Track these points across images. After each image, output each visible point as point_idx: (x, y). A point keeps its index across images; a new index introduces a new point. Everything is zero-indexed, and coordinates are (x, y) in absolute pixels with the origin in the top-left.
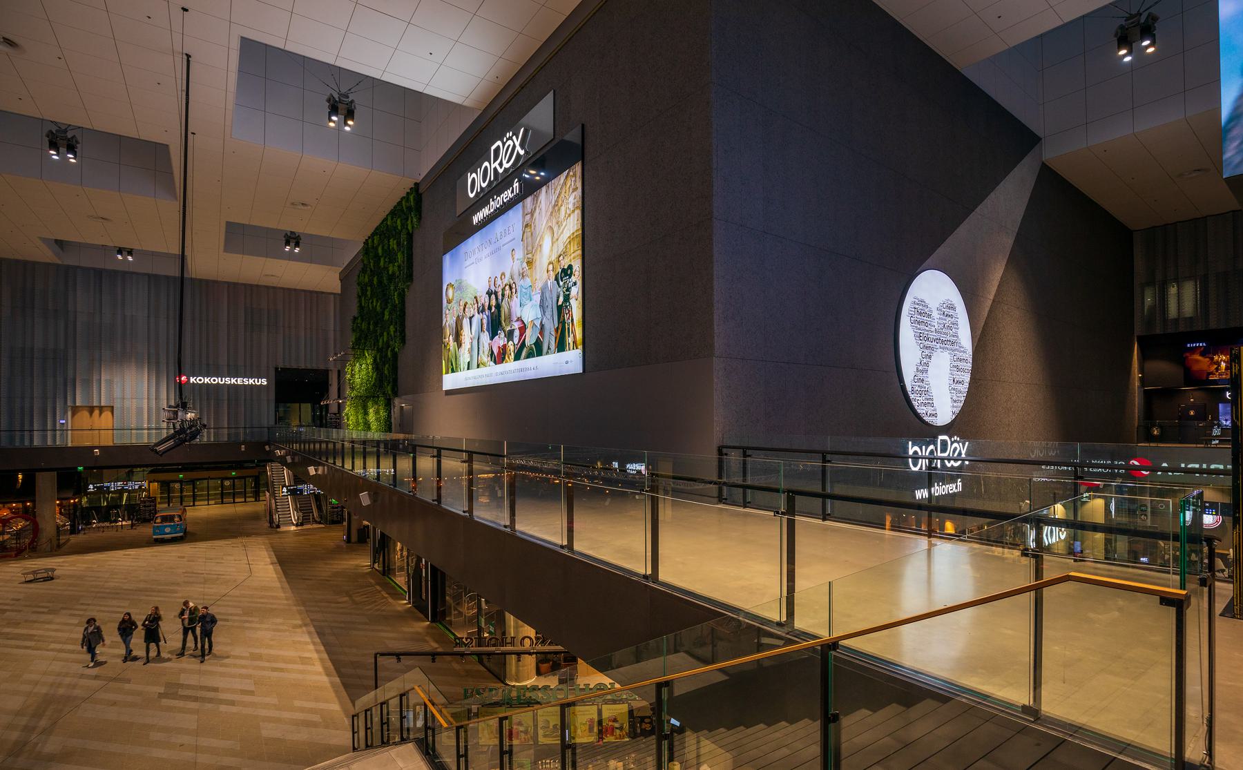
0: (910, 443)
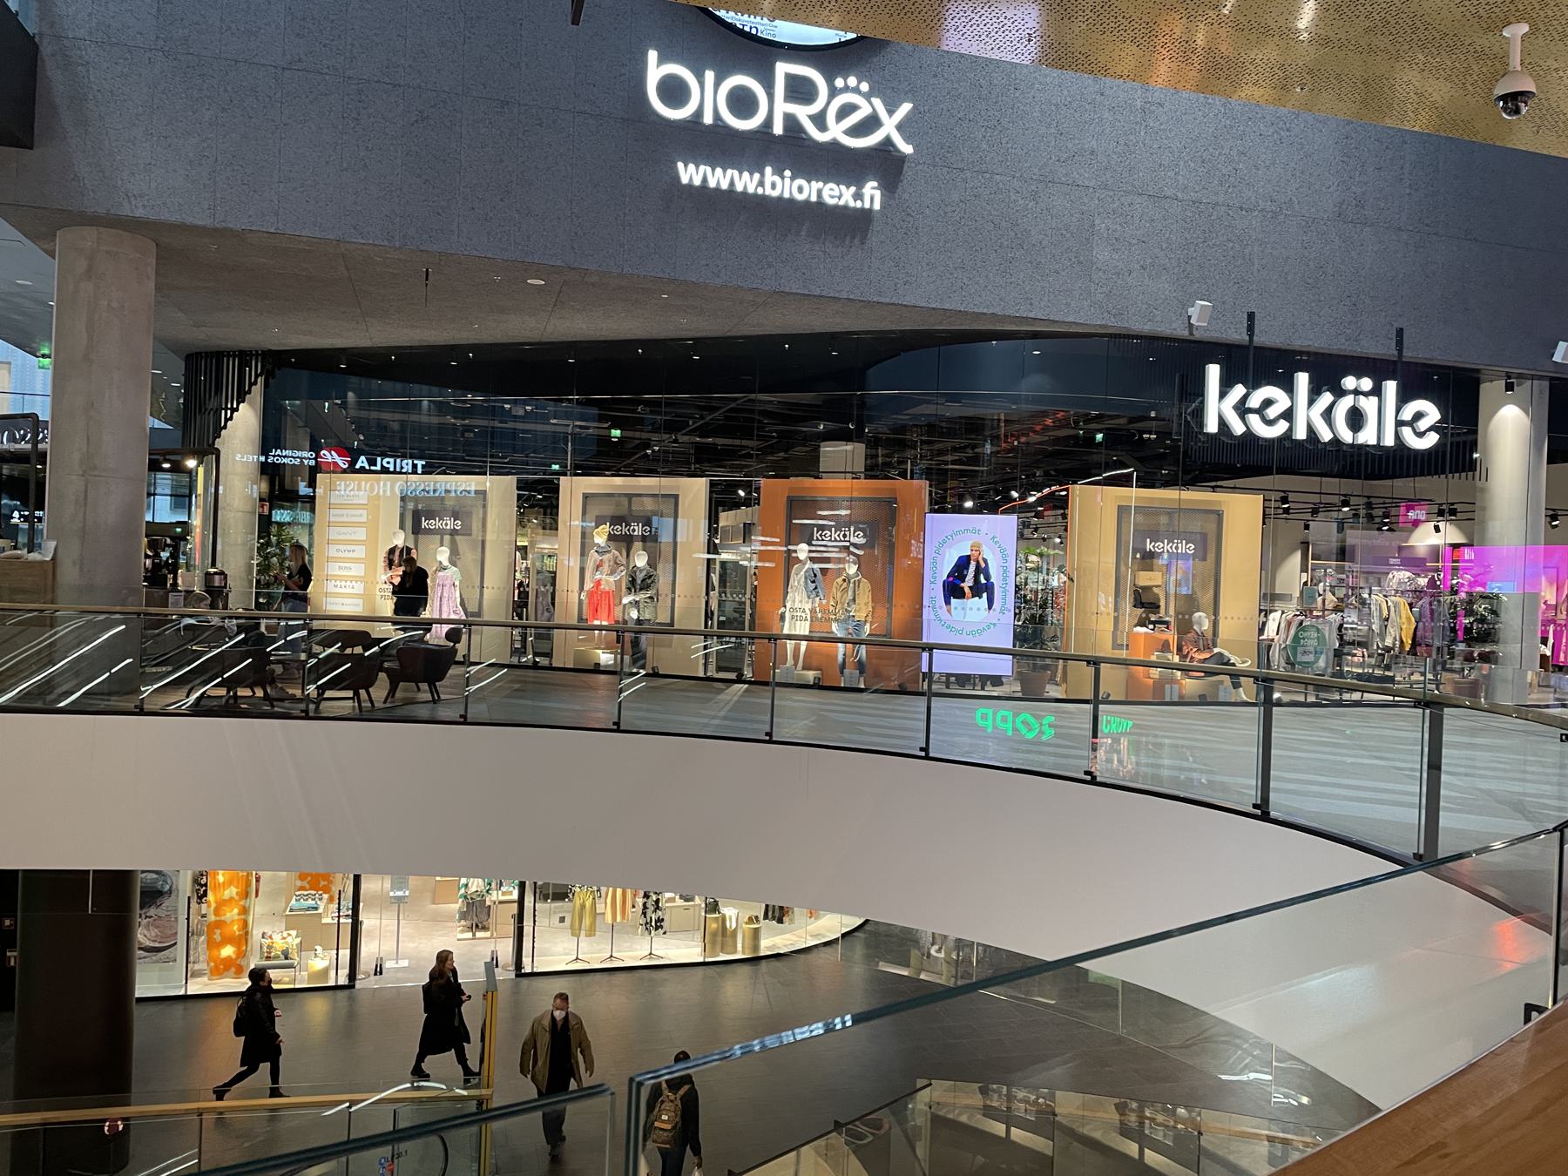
0: (1213, 372)
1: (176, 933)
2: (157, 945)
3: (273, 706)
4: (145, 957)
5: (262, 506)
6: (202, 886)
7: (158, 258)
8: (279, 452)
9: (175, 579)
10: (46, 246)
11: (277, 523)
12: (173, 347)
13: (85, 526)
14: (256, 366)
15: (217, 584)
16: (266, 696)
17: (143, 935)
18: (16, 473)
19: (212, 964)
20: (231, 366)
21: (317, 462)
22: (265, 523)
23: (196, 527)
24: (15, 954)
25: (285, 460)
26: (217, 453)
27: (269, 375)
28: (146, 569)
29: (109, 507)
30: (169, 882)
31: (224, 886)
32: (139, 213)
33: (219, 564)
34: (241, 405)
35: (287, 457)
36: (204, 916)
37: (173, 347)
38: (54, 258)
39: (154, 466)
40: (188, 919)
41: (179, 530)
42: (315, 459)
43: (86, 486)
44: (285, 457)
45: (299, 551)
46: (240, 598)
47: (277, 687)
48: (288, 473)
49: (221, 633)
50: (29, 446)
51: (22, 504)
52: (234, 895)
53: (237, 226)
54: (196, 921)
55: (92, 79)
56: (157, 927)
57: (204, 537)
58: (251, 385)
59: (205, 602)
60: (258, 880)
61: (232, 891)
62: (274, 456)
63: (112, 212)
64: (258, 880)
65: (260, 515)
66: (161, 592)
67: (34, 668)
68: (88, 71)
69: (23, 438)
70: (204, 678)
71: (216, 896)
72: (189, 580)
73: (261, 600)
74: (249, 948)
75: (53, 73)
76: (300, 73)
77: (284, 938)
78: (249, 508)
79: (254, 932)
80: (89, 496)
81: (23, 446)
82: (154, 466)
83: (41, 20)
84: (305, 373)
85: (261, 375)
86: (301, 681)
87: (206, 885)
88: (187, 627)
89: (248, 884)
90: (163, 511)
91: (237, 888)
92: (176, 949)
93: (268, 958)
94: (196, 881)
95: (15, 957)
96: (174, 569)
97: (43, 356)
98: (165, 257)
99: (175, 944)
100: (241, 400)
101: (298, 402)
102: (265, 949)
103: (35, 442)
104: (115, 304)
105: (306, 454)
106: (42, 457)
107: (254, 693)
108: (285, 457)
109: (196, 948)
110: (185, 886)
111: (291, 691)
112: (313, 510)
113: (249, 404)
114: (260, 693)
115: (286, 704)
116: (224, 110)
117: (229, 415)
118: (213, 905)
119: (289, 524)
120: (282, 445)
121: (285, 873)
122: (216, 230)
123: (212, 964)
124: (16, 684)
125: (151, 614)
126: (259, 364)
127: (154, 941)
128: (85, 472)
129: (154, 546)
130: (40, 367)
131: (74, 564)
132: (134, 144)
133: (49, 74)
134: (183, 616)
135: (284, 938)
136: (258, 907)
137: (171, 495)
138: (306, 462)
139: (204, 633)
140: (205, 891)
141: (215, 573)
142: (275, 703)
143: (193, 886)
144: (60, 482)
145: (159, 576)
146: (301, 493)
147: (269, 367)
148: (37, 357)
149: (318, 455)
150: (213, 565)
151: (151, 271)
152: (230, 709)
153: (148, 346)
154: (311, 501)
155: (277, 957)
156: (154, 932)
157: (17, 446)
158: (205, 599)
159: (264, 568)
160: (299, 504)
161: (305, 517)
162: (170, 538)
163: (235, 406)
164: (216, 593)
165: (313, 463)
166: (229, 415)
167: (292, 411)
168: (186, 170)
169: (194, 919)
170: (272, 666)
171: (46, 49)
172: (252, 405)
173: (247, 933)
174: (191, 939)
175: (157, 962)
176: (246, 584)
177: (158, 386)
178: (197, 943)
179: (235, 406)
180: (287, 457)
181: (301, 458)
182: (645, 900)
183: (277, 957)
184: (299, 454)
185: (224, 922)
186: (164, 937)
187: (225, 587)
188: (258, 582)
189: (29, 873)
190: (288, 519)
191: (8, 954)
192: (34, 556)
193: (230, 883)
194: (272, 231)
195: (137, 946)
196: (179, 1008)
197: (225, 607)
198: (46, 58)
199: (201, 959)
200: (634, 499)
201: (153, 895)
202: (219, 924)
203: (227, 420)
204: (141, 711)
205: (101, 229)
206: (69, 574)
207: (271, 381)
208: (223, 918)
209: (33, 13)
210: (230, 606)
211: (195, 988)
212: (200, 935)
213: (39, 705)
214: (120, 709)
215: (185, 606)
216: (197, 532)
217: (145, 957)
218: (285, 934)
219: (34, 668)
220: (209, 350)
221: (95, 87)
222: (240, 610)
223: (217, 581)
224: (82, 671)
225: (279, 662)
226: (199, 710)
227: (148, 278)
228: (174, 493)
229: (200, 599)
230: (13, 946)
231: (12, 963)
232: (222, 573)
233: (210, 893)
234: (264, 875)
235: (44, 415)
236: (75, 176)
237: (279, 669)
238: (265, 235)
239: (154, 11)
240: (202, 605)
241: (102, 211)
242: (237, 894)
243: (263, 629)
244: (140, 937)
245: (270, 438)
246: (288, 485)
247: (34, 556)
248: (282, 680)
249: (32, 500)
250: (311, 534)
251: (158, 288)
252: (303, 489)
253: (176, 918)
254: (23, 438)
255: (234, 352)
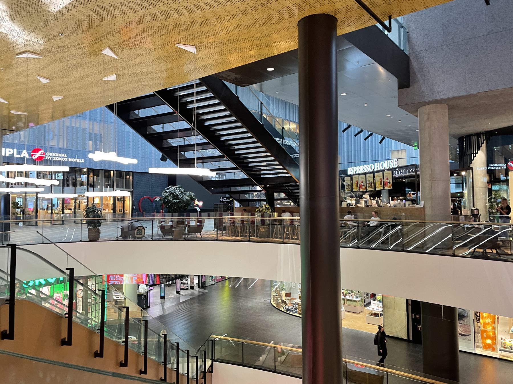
1: (470, 331)
2: (464, 334)
3: (500, 256)
4: (460, 337)
5: (489, 185)
6: (478, 316)
7: (449, 109)
8: (492, 165)
9: (461, 212)
10: (415, 114)
11: (494, 190)
12: (454, 137)
13: (432, 196)
14: (483, 137)
15: (475, 213)
16: (497, 253)
17: (460, 330)
18: (409, 181)
19: (484, 345)
20: (474, 139)
21: (507, 167)
22: (490, 191)
23: (466, 193)
24: (421, 327)
25: (494, 168)
26: (472, 169)
27: (488, 140)
28: (452, 209)
29: (439, 190)
30: (466, 313)
31: (486, 319)
32: (442, 97)
33: (475, 206)
34: (479, 151)
35: (496, 166)
36: (479, 327)
37: (454, 137)
38: (418, 117)
39: (452, 175)
40: (474, 327)
41: (459, 195)
42: (506, 166)
43: (432, 184)
44: (495, 166)
45: (504, 201)
46: (484, 217)
47: (501, 249)
48: (497, 172)
49: (479, 230)
50: (414, 173)
51: (411, 190)
52: (490, 322)
53: (475, 93)
54: (477, 328)
55: (425, 61)
56: (463, 328)
57: (469, 196)
58: (482, 144)
59: (472, 219)
60: (498, 318)
61: (489, 320)
62: (490, 167)
63: (434, 99)
64: (498, 318)
65: (488, 188)
66: (457, 216)
67: (419, 239)
68: (424, 59)
69: (412, 171)
70: (473, 244)
71: (483, 321)
72: (466, 212)
73: (491, 218)
74: (497, 342)
75: (414, 64)
76: (492, 35)
77: (510, 341)
78: (484, 186)
79: (498, 337)
80: (433, 187)
81: (412, 173)
82: (452, 175)
83: (410, 49)
84: (500, 136)
85: (485, 140)
86: (510, 247)
87: (479, 316)
88: (467, 228)
89: (494, 319)
90: (454, 189)
91: (491, 320)
92: (470, 337)
93: (504, 347)
94: (476, 314)
95: (420, 328)
96: (460, 208)
97: (415, 146)
98: (451, 108)
99: (470, 335)
100: (478, 149)
101: (499, 147)
102: (503, 344)
103: (416, 171)
104: (436, 127)
105: (503, 165)
106: (418, 176)
107: (492, 251)
108: (495, 166)
109: (477, 338)
110: (472, 316)
111: (506, 251)
112: (508, 185)
113: (481, 150)
114: (494, 251)
115: (505, 256)
116: (467, 56)
117: (474, 156)
118: (483, 324)
119: (499, 190)
120: (494, 163)
121: (508, 318)
122: (467, 96)
123: (484, 345)
124: (414, 244)
125: (455, 224)
126: (484, 137)
127: (463, 332)
128: (431, 179)
129: (453, 201)
130: (415, 150)
131: (430, 208)
132: (439, 76)
133: (413, 64)
134: (465, 224)
135: (510, 341)
136: (499, 328)
137: (455, 184)
138: (502, 167)
139: (470, 230)
140: (479, 318)
141: (475, 209)
142: (501, 255)
143: (475, 316)
144: (424, 184)
145: (456, 211)
146: (502, 179)
147: (488, 137)
148: (413, 146)
149: (507, 165)
150: (474, 206)
151: (447, 114)
152: (484, 256)
153: (447, 138)
154: (507, 182)
155: (507, 348)
156: (463, 329)
157: (411, 174)
158: (472, 218)
159: (491, 207)
160: (501, 183)
161: (505, 187)
162: (457, 198)
163: (476, 152)
164: (475, 216)
165: (505, 167)
166: (474, 156)
167: (497, 151)
168: (456, 79)
169: (476, 328)
170: (499, 242)
171: (411, 57)
172: (482, 151)
173: (495, 336)
174: (475, 334)
175: (464, 339)
176: (485, 212)
177: (451, 149)
178: (478, 336)
179: (476, 152)
180: (496, 166)
181: (501, 166)
182: (493, 330)
183: (507, 348)
184: (500, 165)
185: (487, 331)
186: (466, 332)
187: (478, 214)
188: (489, 212)
189: (424, 303)
190: (498, 188)
191: (418, 326)
192: (418, 206)
193: (488, 317)
194: (487, 90)
195: (458, 333)
196: (473, 357)
197: (479, 221)
198: (411, 60)
199: (480, 342)
200: (376, 174)
201: (462, 317)
202: (485, 331)
203: (474, 157)
204: (454, 255)
205: (431, 105)
206: (428, 211)
207: (489, 141)
208: (486, 329)
209: (408, 48)
210: (481, 220)
211: (478, 351)
212: (478, 333)
213: (421, 251)
214: (448, 254)
215: (465, 221)
216: (466, 197)
217: (460, 337)
218: (510, 340)
219: (419, 239)
220: (466, 135)
221: (426, 63)
222: (484, 222)
223: (475, 212)
224: (434, 240)
225: (501, 241)
226: (473, 256)
227: (446, 116)
228: (456, 183)
229: (470, 218)
230: (420, 324)
231: (420, 329)
232: (477, 209)
233: (481, 319)
234: (500, 317)
235: (418, 163)
236: (423, 91)
237: (501, 243)
238: (484, 93)
239: (442, 34)
240: (471, 220)
241: (431, 100)
242: (491, 322)
243: (493, 229)
244: (459, 330)
245: (490, 160)
246: (497, 177)
247: (418, 206)
248: (502, 247)
249: (416, 189)
250: (507, 193)
251: (449, 119)
252: (503, 177)
253: (470, 326)
254: (412, 171)
255: (475, 134)
